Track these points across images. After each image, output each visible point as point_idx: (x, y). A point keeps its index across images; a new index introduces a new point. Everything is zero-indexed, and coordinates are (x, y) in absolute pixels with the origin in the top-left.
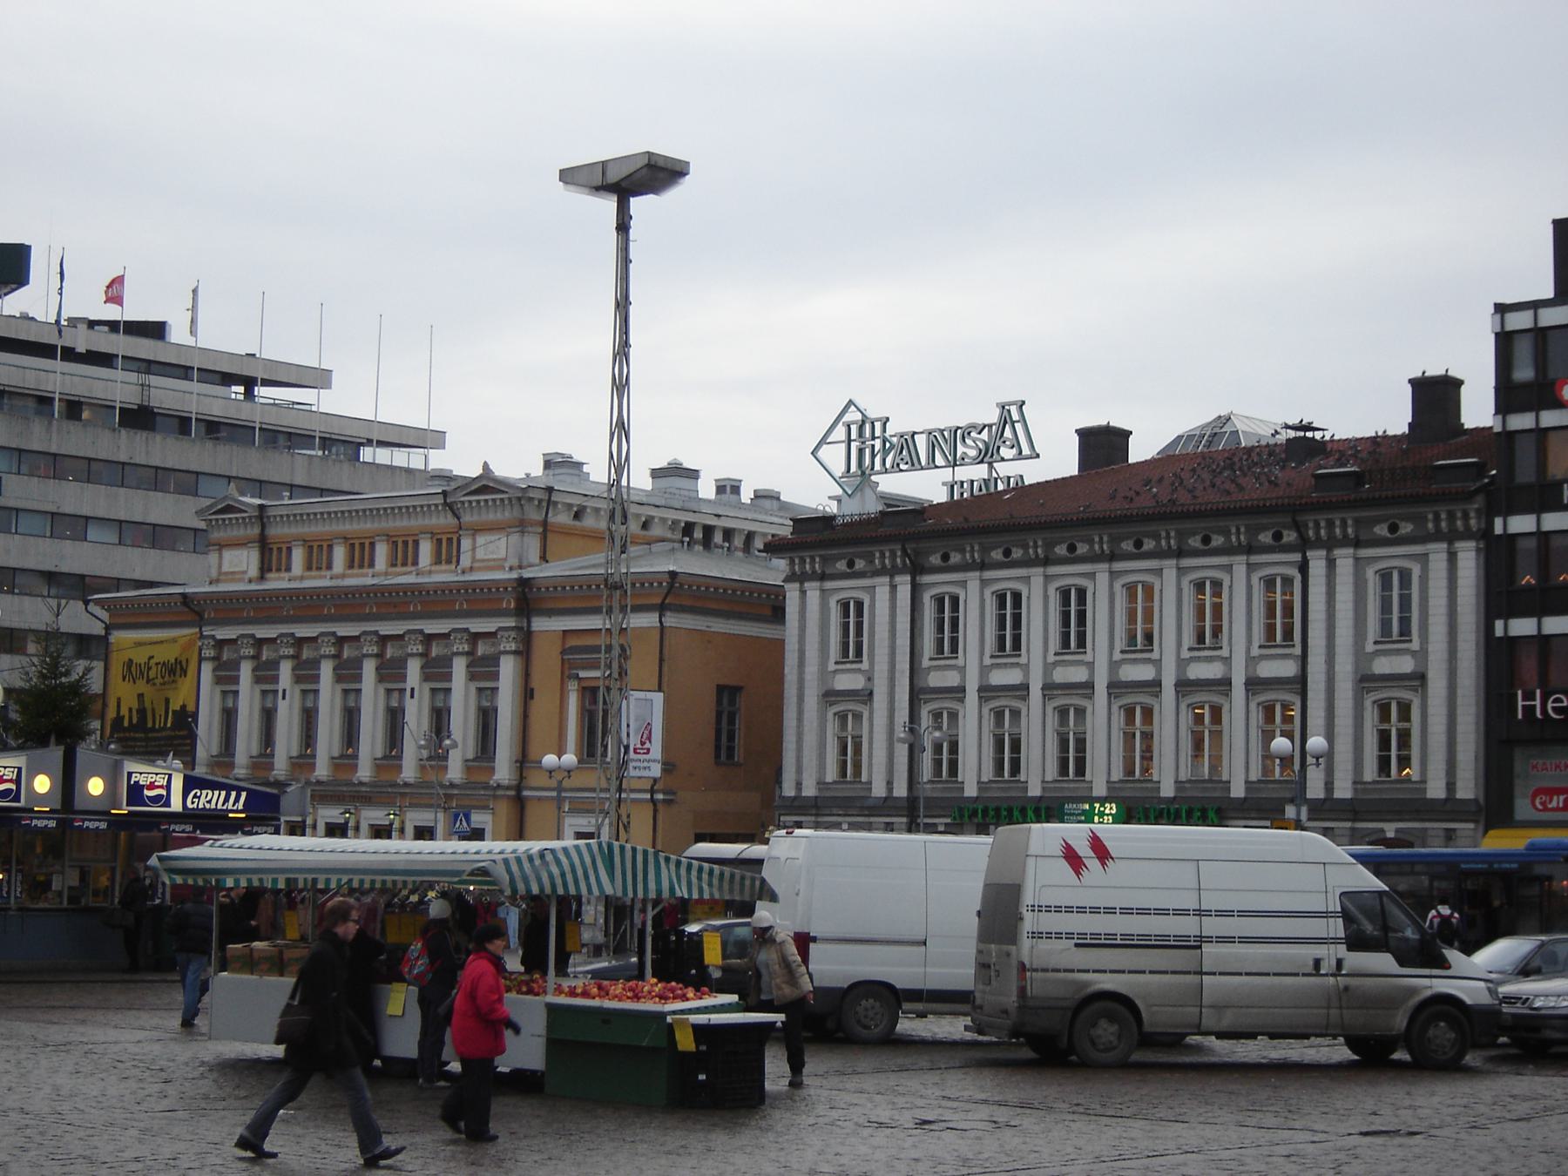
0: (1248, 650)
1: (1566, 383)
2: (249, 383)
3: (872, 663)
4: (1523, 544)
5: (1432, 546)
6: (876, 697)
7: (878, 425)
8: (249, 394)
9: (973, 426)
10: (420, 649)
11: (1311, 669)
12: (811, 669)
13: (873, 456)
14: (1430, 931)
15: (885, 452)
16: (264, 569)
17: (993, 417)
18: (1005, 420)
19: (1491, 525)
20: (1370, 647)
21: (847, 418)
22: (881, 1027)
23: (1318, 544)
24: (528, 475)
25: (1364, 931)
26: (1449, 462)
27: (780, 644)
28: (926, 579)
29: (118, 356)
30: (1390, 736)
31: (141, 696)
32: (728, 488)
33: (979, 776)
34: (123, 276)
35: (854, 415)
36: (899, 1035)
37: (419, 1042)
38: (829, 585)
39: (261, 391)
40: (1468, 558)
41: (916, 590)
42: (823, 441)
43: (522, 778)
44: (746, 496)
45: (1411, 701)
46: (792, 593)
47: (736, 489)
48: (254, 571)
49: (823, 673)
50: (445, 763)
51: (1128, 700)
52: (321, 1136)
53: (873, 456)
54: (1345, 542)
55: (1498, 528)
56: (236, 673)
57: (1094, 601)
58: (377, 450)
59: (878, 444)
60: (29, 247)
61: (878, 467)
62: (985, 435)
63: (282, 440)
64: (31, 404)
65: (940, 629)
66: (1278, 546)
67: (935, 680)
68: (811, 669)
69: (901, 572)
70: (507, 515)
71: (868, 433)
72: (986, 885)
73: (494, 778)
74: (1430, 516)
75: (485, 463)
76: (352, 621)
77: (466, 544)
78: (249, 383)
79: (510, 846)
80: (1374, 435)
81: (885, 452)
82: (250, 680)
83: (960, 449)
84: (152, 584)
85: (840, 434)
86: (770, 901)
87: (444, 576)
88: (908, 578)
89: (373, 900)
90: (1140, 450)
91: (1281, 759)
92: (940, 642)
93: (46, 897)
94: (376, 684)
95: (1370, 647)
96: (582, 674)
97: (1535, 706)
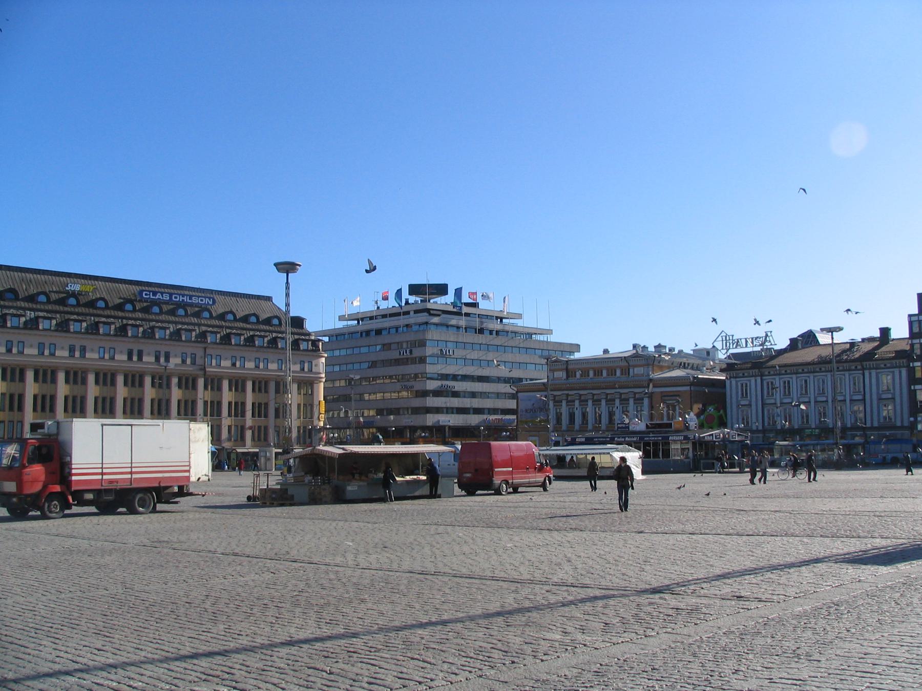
0: (850, 393)
2: (501, 319)
3: (751, 397)
4: (917, 368)
5: (896, 369)
6: (753, 406)
7: (731, 337)
8: (501, 321)
9: (758, 337)
12: (734, 400)
13: (730, 344)
15: (733, 344)
16: (568, 377)
17: (764, 335)
18: (767, 335)
19: (910, 365)
20: (816, 395)
21: (722, 335)
23: (866, 369)
24: (606, 351)
27: (725, 394)
28: (764, 378)
35: (723, 334)
38: (738, 379)
39: (504, 320)
40: (904, 372)
41: (762, 381)
42: (715, 341)
44: (676, 352)
46: (728, 383)
47: (674, 349)
48: (565, 376)
49: (737, 401)
53: (730, 344)
54: (874, 368)
55: (911, 365)
58: (73, 463)
59: (731, 341)
60: (447, 285)
61: (731, 347)
62: (761, 339)
63: (450, 411)
64: (455, 328)
65: (746, 390)
66: (856, 369)
67: (768, 401)
68: (734, 400)
69: (758, 376)
70: (643, 362)
71: (728, 339)
75: (276, 265)
77: (631, 370)
78: (501, 319)
81: (733, 344)
83: (755, 343)
84: (536, 380)
85: (720, 338)
87: (624, 378)
88: (760, 378)
92: (743, 394)
95: (739, 399)
96: (668, 402)
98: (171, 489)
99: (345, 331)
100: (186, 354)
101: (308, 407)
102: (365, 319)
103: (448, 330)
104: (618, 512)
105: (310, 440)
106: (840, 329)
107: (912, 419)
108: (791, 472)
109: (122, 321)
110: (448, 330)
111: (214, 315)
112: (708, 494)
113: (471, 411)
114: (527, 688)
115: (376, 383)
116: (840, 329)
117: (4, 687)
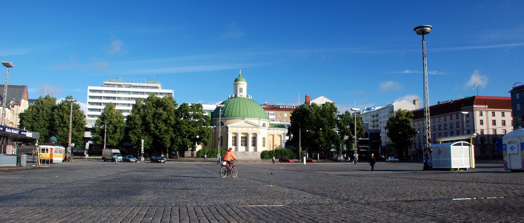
24: (439, 102)
33: (150, 162)
63: (443, 142)
108: (415, 130)
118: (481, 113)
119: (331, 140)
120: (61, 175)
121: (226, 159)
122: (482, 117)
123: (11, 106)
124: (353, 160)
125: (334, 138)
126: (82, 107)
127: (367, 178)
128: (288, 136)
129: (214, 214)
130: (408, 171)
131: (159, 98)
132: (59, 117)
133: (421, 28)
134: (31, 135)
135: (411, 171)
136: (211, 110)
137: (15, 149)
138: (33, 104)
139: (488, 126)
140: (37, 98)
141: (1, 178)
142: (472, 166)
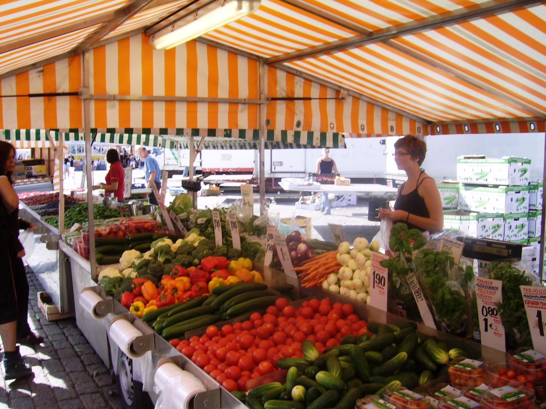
1: (10, 405)
10: (92, 105)
11: (137, 189)
14: (473, 288)
17: (332, 211)
22: (517, 239)
24: (170, 203)
25: (434, 234)
26: (14, 283)
29: (337, 185)
30: (65, 138)
31: (33, 150)
32: (223, 169)
33: (503, 163)
34: (330, 214)
36: (343, 295)
37: (425, 157)
43: (191, 287)
45: (106, 170)
50: (273, 179)
51: (383, 287)
52: (520, 187)
56: (273, 179)
57: (84, 63)
58: (273, 150)
63: (481, 127)
72: (521, 132)
73: (140, 261)
74: (116, 178)
76: (71, 275)
79: (38, 217)
80: (394, 157)
82: (460, 253)
86: (298, 148)
89: (198, 179)
90: (279, 183)
91: (169, 275)
93: (490, 365)
94: (461, 255)
97: (408, 404)
98: (53, 319)
99: (141, 265)
100: (333, 124)
101: (96, 222)
102: (140, 185)
103: (160, 392)
104: (89, 272)
105: (351, 215)
106: (542, 334)
107: (227, 318)
108: (75, 196)
109: (50, 268)
110: (160, 392)
111: (239, 382)
112: (485, 208)
113: (375, 180)
114: (539, 202)
115: (385, 406)
116: (542, 334)
117: (508, 186)
118: (489, 186)
119: (436, 392)
120: (335, 351)
121: (396, 192)
122: (345, 149)
123: (225, 238)
124: (522, 279)
125: (460, 265)
126: (51, 314)
127: (385, 403)
128: (44, 242)
129: (328, 150)
130: (474, 83)
131: (368, 230)
132: (498, 296)
133: (435, 314)
134: (269, 230)
135: (291, 174)
136: (119, 355)
137: (307, 199)
138: (13, 164)
139: (223, 47)
140: (487, 219)
141: (1, 178)
142: (447, 219)
